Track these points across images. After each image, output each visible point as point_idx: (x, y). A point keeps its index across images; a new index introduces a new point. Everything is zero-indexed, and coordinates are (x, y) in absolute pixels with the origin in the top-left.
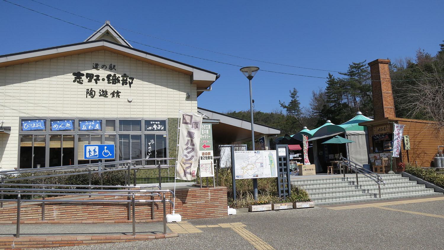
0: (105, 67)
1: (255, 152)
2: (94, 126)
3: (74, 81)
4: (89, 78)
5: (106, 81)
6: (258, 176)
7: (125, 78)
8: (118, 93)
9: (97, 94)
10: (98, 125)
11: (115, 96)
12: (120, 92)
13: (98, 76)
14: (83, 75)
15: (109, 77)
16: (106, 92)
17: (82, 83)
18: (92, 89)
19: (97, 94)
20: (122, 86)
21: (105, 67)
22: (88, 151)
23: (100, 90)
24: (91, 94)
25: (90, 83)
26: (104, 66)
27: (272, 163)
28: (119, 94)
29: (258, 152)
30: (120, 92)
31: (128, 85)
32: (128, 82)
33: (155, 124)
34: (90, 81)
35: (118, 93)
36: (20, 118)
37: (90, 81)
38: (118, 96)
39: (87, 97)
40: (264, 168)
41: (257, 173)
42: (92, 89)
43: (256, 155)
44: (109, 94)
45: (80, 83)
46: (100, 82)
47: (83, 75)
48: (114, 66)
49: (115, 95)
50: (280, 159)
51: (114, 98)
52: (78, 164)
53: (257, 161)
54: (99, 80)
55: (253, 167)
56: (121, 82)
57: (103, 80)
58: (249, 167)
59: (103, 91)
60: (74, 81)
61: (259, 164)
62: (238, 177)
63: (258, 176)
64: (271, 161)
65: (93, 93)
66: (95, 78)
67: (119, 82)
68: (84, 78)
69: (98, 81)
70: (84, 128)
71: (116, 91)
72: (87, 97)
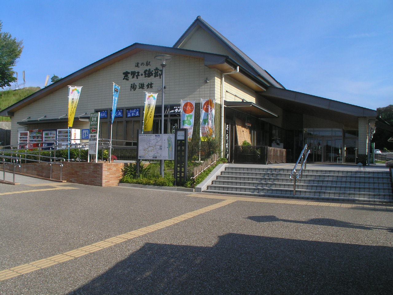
0: (143, 64)
1: (156, 136)
2: (135, 113)
3: (124, 79)
4: (132, 75)
5: (144, 76)
6: (156, 158)
7: (157, 71)
8: (151, 84)
9: (138, 87)
10: (138, 112)
11: (149, 88)
12: (153, 84)
13: (138, 73)
14: (129, 73)
15: (145, 72)
16: (144, 85)
17: (128, 80)
18: (134, 83)
19: (138, 87)
20: (154, 78)
21: (143, 64)
22: (83, 133)
23: (140, 84)
24: (134, 88)
25: (134, 79)
26: (142, 63)
27: (170, 146)
28: (153, 85)
29: (158, 135)
30: (153, 84)
31: (159, 77)
32: (158, 74)
33: (177, 108)
34: (133, 77)
35: (151, 84)
36: (95, 110)
37: (133, 77)
38: (151, 87)
39: (131, 90)
40: (163, 150)
41: (156, 155)
42: (134, 83)
43: (157, 138)
44: (145, 86)
45: (127, 80)
46: (140, 77)
47: (129, 73)
48: (149, 62)
49: (150, 86)
50: (176, 140)
51: (148, 89)
52: (126, 146)
53: (157, 144)
54: (139, 75)
55: (153, 149)
56: (154, 75)
57: (142, 75)
58: (150, 149)
59: (141, 84)
60: (124, 79)
61: (159, 147)
62: (140, 157)
63: (156, 158)
64: (169, 145)
65: (135, 87)
66: (136, 74)
67: (152, 75)
68: (129, 75)
69: (138, 77)
70: (129, 115)
71: (150, 83)
72: (131, 90)
